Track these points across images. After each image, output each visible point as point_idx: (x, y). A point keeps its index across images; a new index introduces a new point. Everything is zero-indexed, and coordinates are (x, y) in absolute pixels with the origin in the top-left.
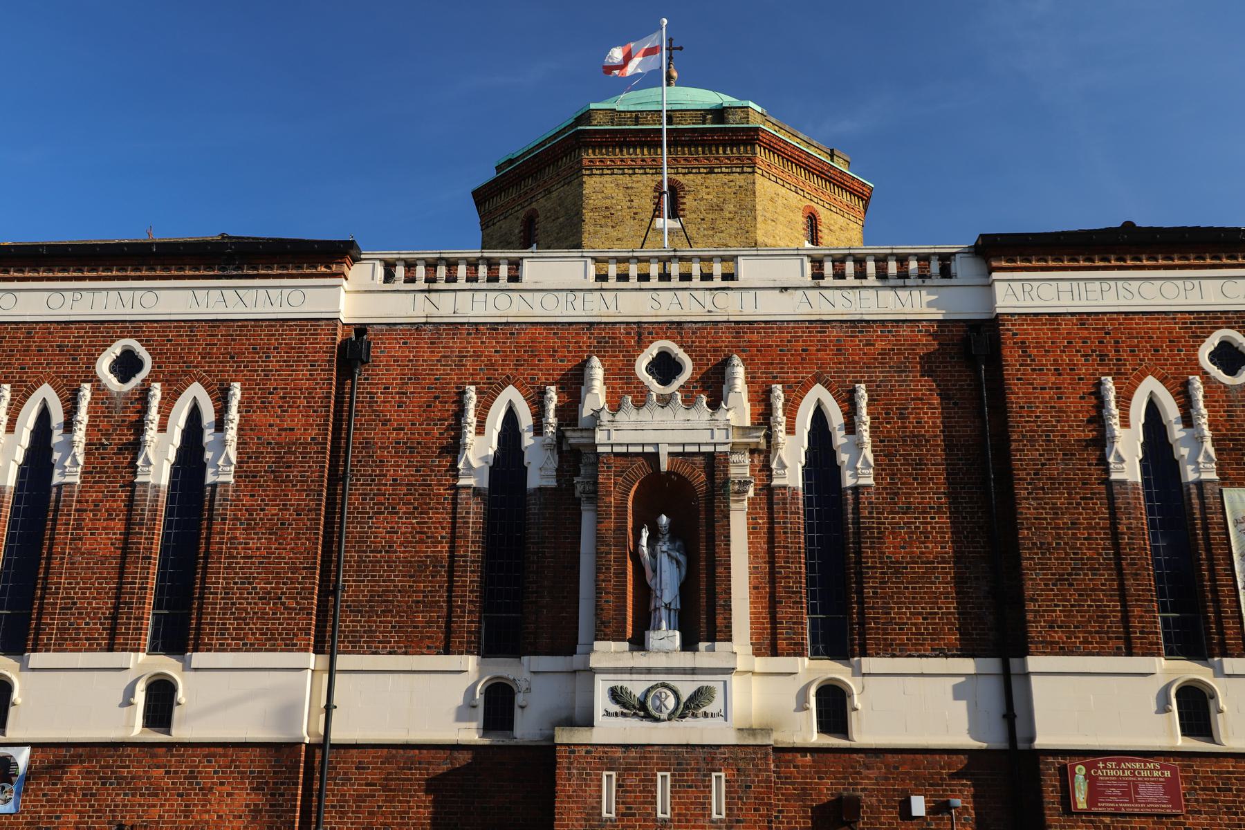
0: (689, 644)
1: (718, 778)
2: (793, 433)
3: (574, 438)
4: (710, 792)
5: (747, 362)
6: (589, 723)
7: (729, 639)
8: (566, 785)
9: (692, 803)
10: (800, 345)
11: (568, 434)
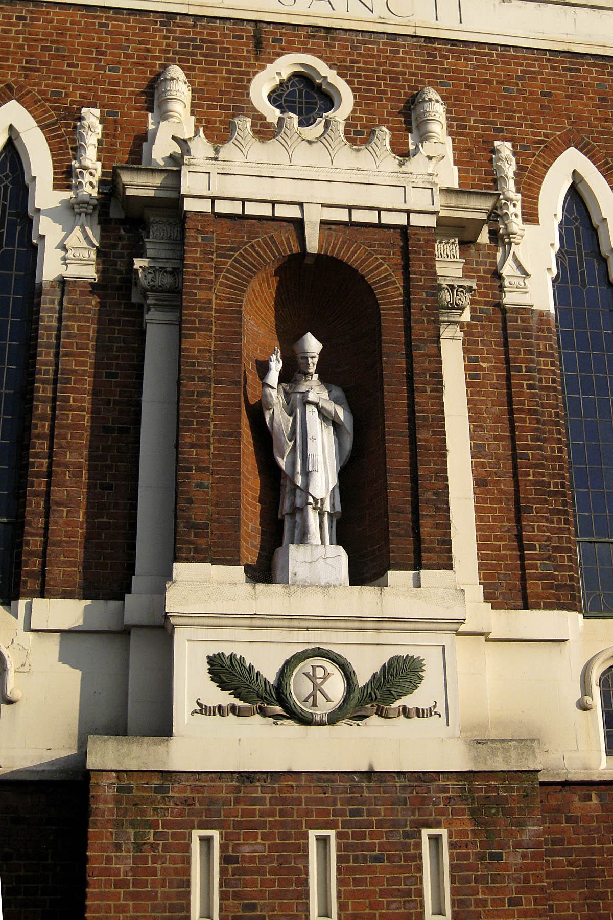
0: (365, 572)
1: (436, 840)
2: (536, 222)
3: (139, 186)
4: (420, 869)
5: (452, 102)
6: (163, 727)
7: (449, 566)
8: (109, 852)
9: (383, 893)
10: (538, 87)
11: (126, 178)
